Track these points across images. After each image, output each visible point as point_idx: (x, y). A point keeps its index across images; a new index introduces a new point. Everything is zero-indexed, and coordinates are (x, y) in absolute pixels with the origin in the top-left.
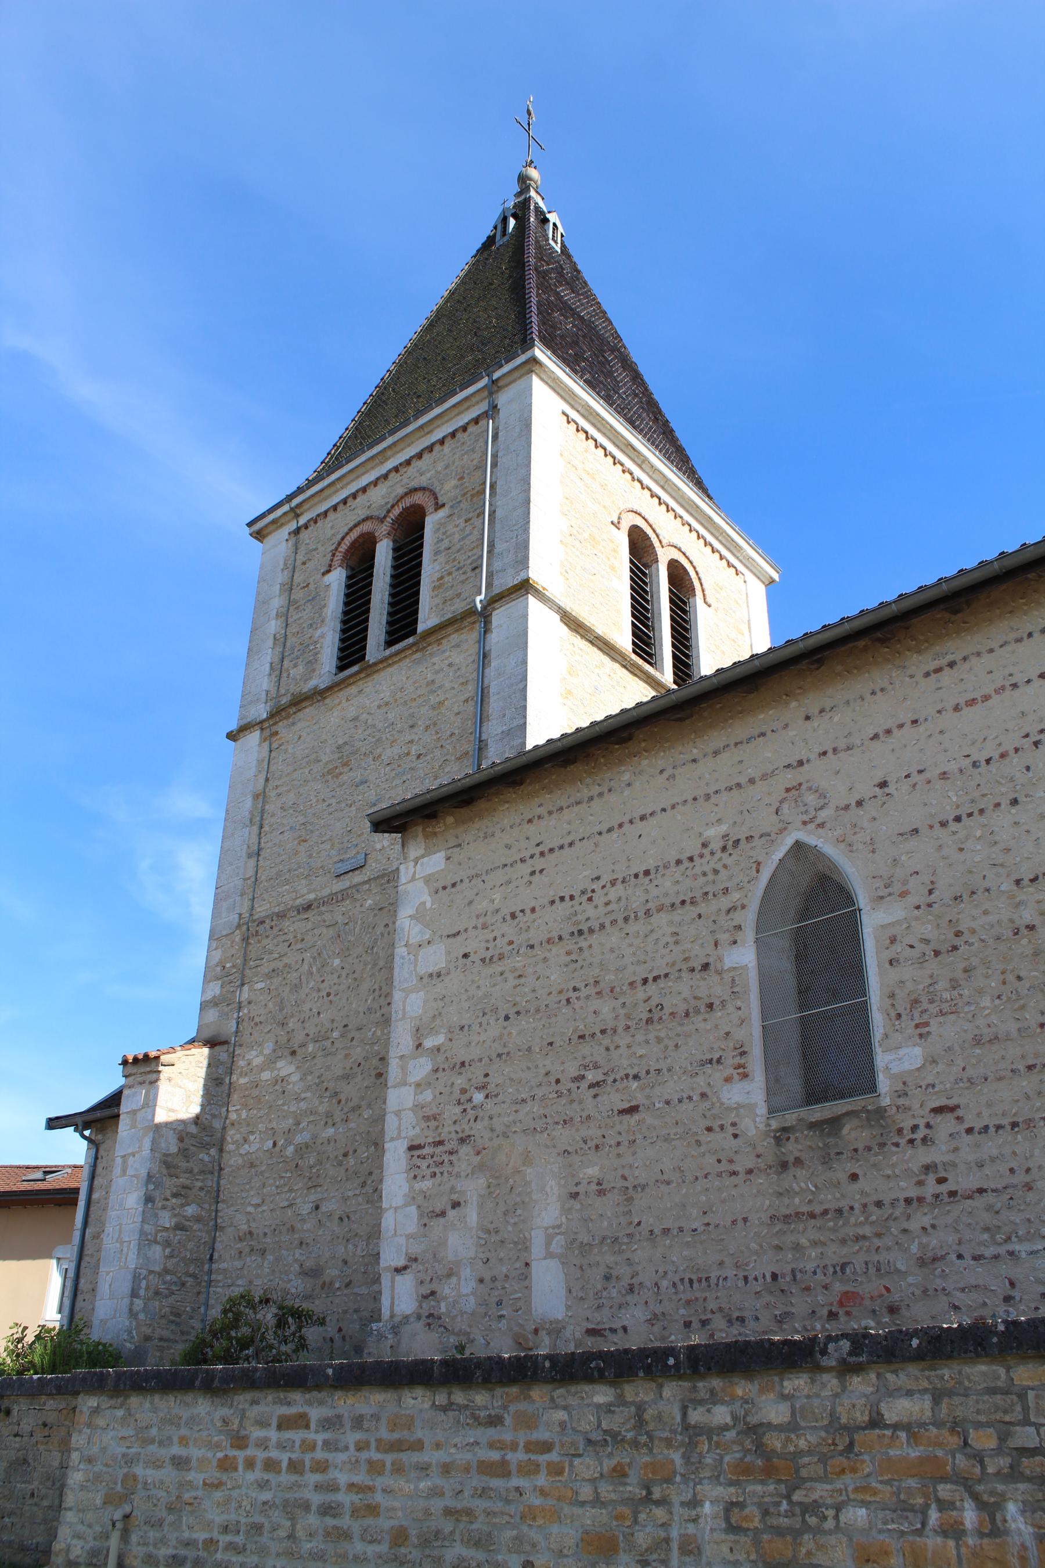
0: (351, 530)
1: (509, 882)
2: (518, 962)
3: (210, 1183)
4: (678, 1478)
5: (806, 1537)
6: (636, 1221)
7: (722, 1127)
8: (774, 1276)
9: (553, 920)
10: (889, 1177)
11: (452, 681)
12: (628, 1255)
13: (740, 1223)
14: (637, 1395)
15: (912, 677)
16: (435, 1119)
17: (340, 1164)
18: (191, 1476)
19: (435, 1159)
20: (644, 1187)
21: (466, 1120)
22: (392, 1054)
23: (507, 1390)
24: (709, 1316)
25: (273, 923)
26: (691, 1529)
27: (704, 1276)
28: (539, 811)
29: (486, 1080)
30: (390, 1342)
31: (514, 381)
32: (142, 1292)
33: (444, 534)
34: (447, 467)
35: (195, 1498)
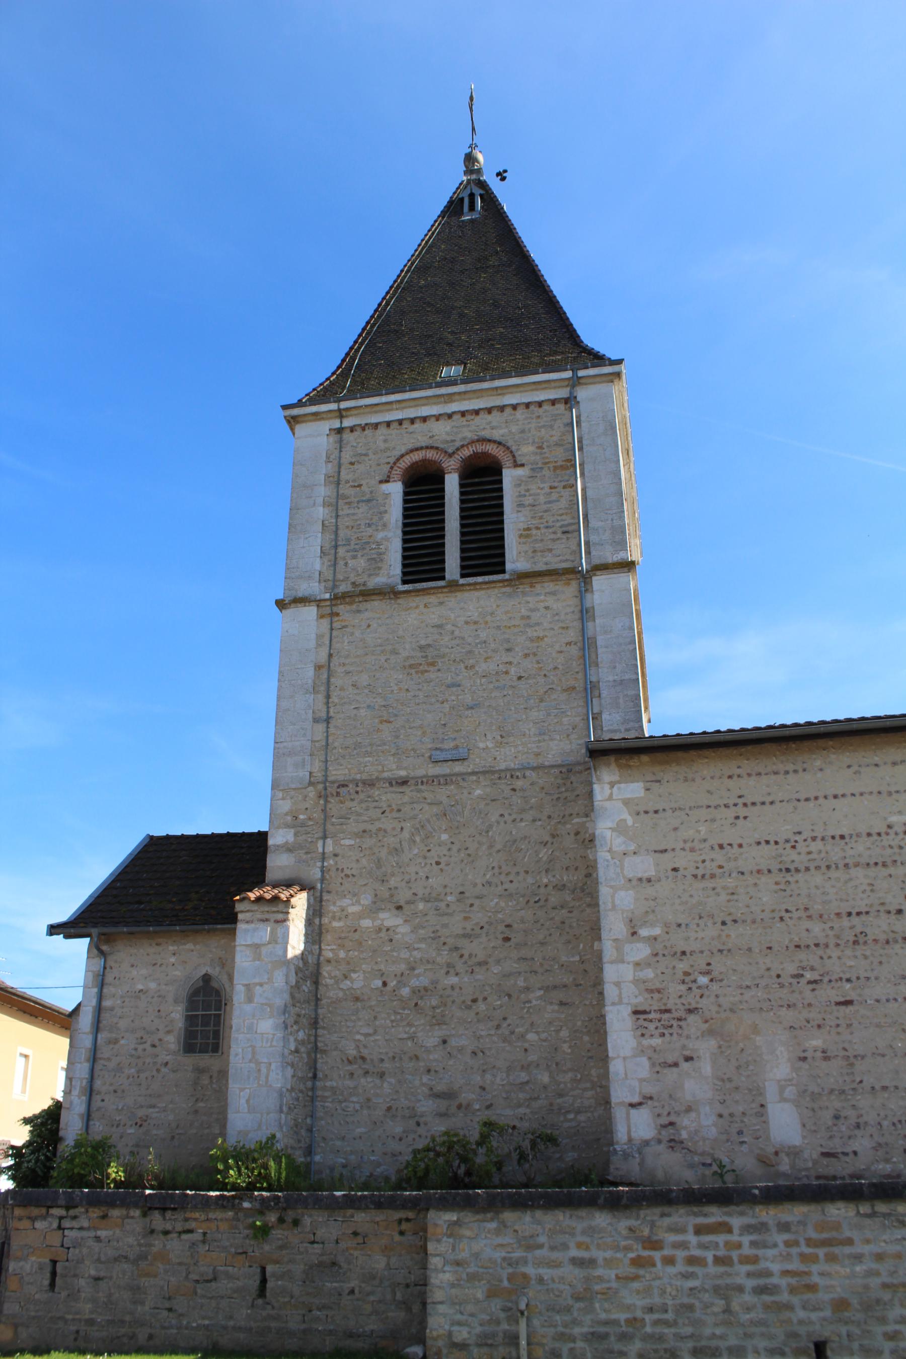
0: (412, 451)
1: (713, 820)
2: (730, 882)
6: (858, 1080)
9: (762, 856)
11: (550, 623)
12: (854, 1103)
17: (469, 1008)
18: (599, 1272)
19: (662, 1022)
20: (863, 1057)
25: (358, 789)
28: (739, 771)
31: (594, 383)
34: (523, 431)
35: (609, 1289)
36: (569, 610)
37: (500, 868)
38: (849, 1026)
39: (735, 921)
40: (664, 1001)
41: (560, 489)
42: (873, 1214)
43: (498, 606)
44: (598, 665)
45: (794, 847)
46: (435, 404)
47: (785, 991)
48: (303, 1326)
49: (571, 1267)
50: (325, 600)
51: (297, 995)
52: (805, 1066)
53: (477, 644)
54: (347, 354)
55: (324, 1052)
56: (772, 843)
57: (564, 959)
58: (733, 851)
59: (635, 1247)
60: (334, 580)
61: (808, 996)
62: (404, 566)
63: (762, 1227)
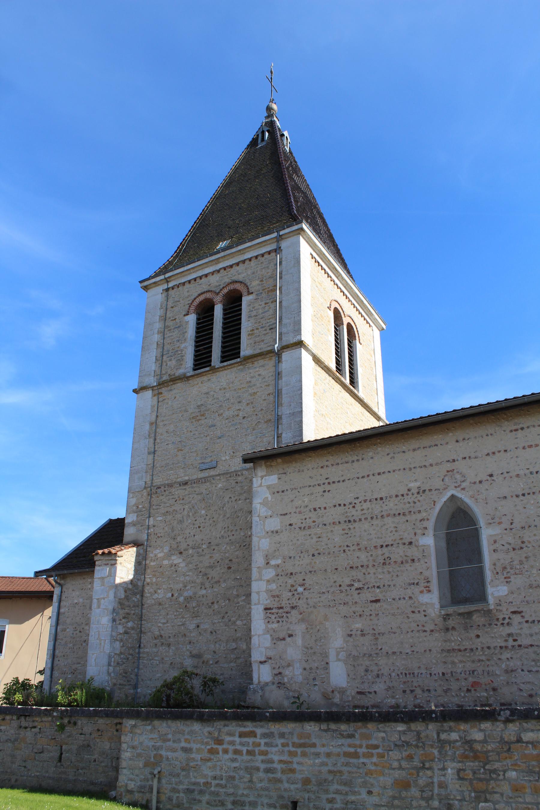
0: (199, 295)
1: (312, 494)
2: (318, 531)
3: (137, 611)
4: (436, 760)
5: (492, 782)
6: (380, 648)
7: (419, 612)
8: (443, 674)
9: (336, 514)
10: (493, 637)
13: (428, 652)
14: (417, 727)
15: (504, 431)
16: (278, 597)
17: (210, 607)
18: (193, 756)
19: (279, 615)
20: (383, 634)
21: (294, 599)
22: (253, 565)
23: (356, 724)
24: (414, 688)
25: (166, 489)
26: (442, 779)
27: (412, 672)
29: (304, 582)
30: (260, 694)
32: (112, 664)
33: (253, 308)
34: (253, 273)
35: (197, 765)
36: (270, 374)
39: (319, 554)
43: (236, 377)
45: (354, 507)
46: (211, 266)
47: (343, 594)
49: (181, 752)
50: (155, 386)
55: (145, 633)
56: (342, 505)
58: (321, 512)
59: (210, 743)
61: (356, 597)
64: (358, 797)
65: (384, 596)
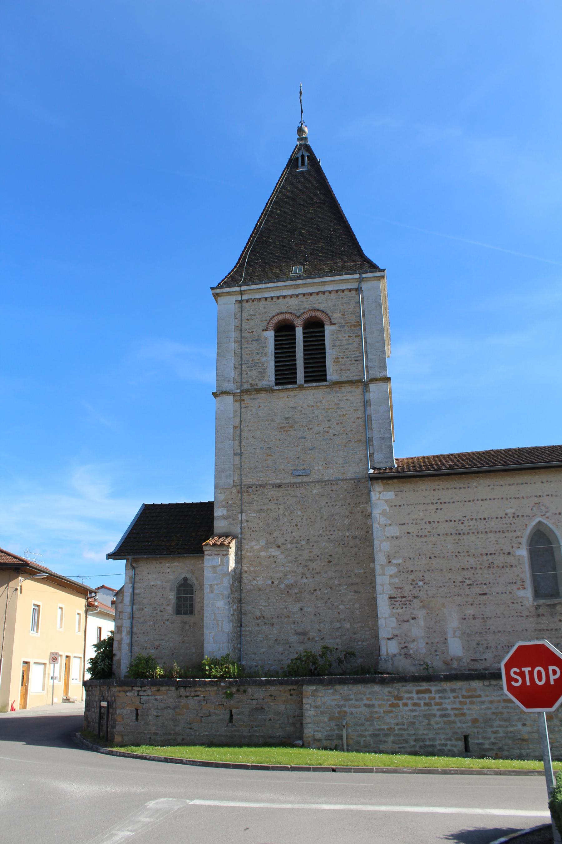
0: (278, 314)
1: (426, 510)
2: (434, 539)
17: (313, 594)
20: (490, 618)
25: (257, 489)
28: (438, 487)
34: (335, 306)
37: (326, 528)
38: (485, 604)
39: (435, 557)
40: (403, 593)
41: (353, 338)
42: (490, 685)
44: (372, 428)
45: (462, 523)
47: (457, 588)
48: (249, 734)
51: (233, 589)
52: (465, 622)
53: (313, 417)
54: (241, 255)
55: (245, 614)
56: (453, 521)
57: (356, 571)
60: (241, 382)
62: (276, 375)
63: (444, 691)
64: (515, 728)
65: (490, 591)
